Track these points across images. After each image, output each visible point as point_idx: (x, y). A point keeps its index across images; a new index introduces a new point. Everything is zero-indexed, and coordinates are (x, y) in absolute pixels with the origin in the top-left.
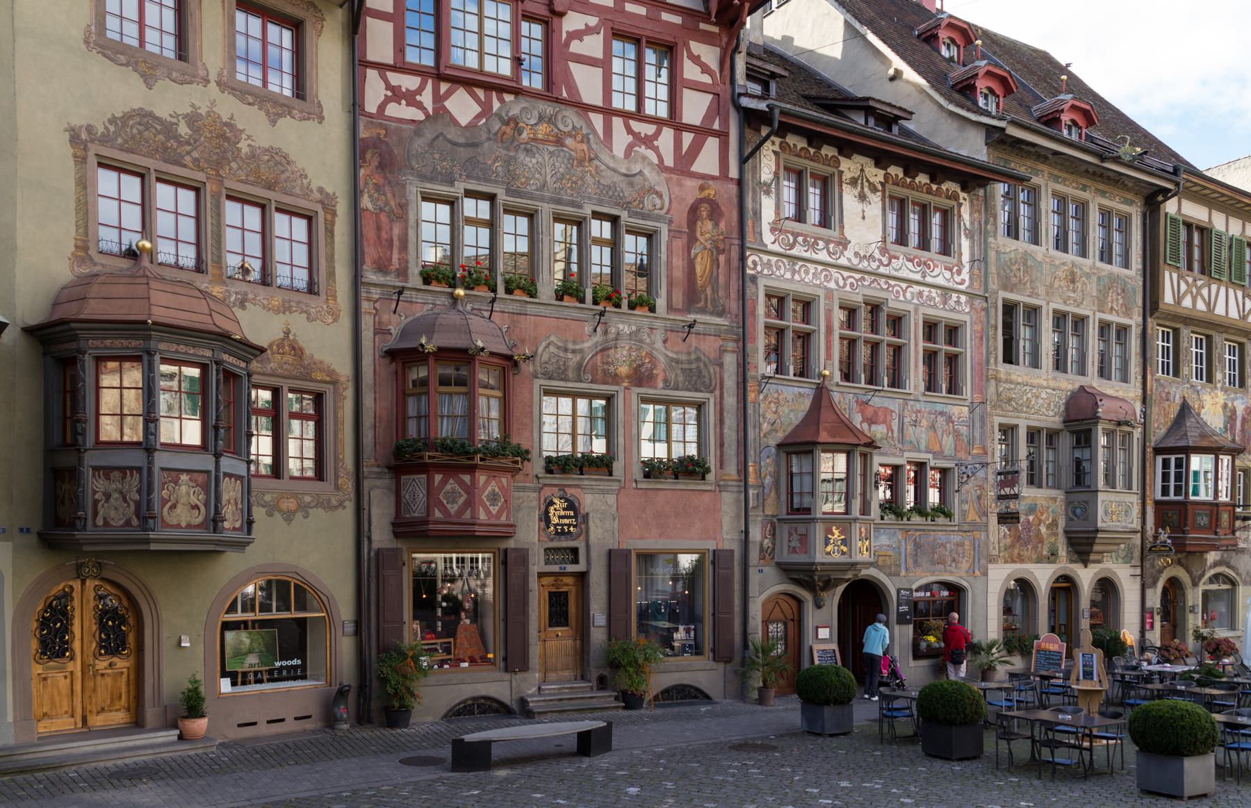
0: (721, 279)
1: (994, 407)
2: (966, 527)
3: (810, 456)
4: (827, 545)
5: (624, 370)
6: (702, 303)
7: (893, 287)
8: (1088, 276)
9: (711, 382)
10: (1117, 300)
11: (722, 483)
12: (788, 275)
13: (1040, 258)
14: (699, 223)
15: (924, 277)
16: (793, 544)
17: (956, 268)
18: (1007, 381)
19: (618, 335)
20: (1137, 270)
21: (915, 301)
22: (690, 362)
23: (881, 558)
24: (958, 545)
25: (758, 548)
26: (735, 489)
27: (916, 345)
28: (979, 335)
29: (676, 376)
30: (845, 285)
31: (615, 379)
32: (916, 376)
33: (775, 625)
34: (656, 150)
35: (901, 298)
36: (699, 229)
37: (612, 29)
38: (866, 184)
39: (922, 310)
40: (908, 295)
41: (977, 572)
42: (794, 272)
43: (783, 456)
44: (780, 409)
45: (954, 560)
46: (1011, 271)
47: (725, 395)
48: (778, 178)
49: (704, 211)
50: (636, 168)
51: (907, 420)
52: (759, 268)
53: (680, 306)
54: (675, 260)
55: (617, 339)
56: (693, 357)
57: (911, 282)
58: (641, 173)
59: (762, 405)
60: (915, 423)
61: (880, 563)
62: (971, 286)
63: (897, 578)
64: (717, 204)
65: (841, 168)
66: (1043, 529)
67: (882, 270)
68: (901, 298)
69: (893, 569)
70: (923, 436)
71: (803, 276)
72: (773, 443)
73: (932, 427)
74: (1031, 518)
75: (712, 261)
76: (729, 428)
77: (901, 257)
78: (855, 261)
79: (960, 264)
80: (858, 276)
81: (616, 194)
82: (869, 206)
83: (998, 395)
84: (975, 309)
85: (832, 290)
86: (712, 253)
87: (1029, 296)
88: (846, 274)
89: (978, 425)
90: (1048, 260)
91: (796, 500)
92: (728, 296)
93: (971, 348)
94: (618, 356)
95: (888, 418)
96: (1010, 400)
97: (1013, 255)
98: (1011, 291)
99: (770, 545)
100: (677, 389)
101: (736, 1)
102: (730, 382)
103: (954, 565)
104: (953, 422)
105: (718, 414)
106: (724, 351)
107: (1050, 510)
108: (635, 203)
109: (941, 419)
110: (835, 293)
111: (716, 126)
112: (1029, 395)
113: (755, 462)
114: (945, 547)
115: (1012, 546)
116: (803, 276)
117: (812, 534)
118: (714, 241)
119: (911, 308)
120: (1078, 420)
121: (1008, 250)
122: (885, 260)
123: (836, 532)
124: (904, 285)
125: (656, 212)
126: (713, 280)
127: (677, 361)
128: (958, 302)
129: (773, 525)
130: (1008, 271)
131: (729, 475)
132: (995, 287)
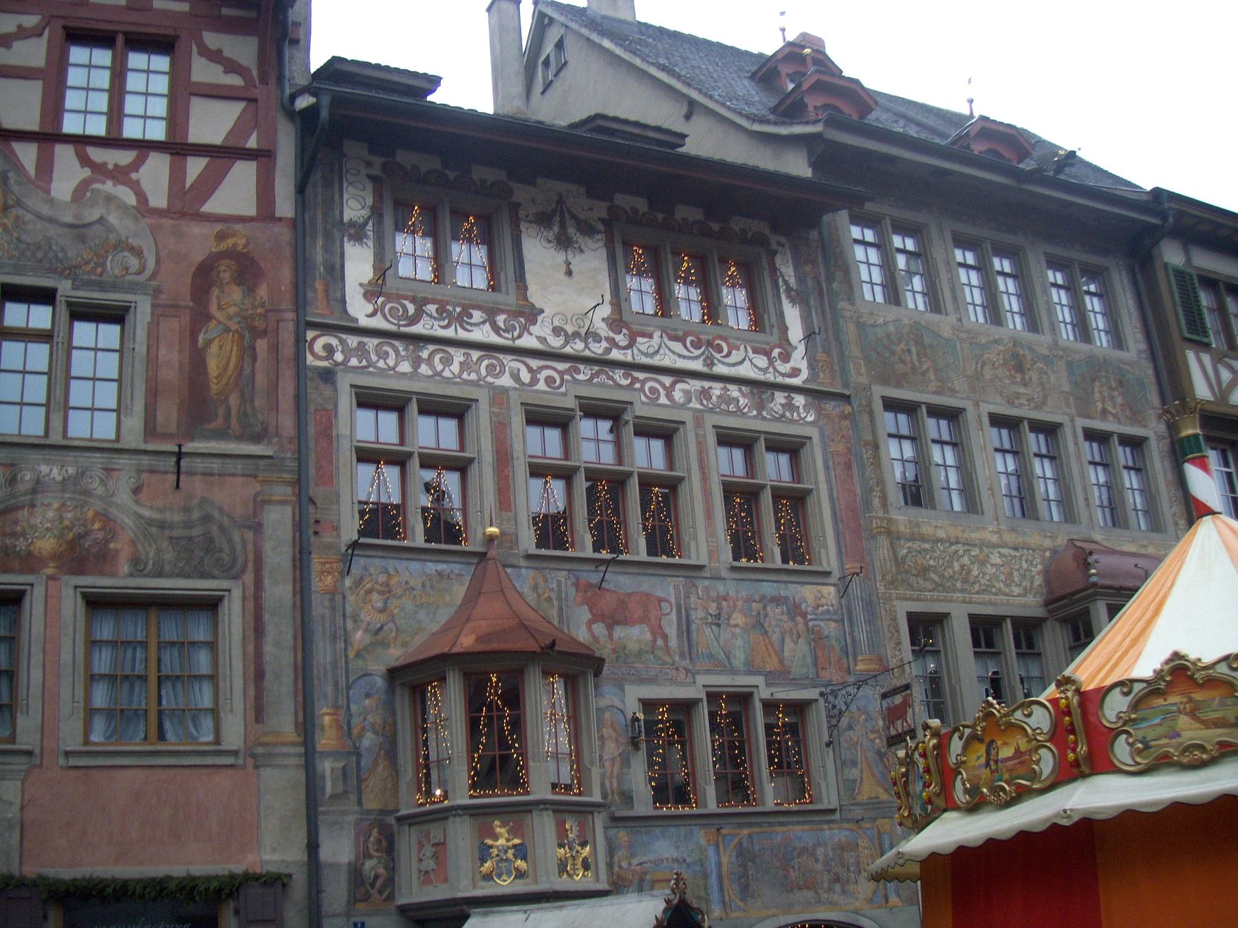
0: (261, 380)
1: (892, 583)
2: (858, 812)
4: (483, 860)
5: (46, 545)
6: (220, 421)
7: (643, 382)
8: (1047, 360)
9: (234, 560)
10: (1112, 398)
11: (260, 750)
12: (405, 367)
13: (947, 332)
14: (215, 292)
15: (710, 362)
17: (776, 352)
18: (913, 538)
19: (38, 486)
20: (1140, 352)
21: (695, 404)
22: (188, 525)
24: (842, 848)
25: (344, 877)
28: (841, 460)
29: (159, 551)
30: (534, 381)
31: (30, 562)
32: (711, 533)
34: (136, 188)
35: (663, 400)
36: (214, 301)
37: (65, 28)
38: (567, 216)
39: (711, 420)
40: (678, 395)
42: (417, 363)
43: (403, 703)
44: (393, 603)
45: (837, 879)
46: (893, 353)
47: (266, 581)
48: (381, 216)
49: (225, 272)
50: (93, 214)
51: (697, 615)
52: (339, 357)
53: (173, 429)
54: (163, 352)
55: (34, 491)
56: (196, 515)
57: (681, 374)
58: (101, 220)
59: (351, 598)
60: (717, 621)
64: (252, 259)
67: (616, 355)
68: (663, 400)
70: (739, 642)
71: (439, 367)
72: (378, 667)
73: (759, 625)
77: (657, 334)
78: (556, 342)
79: (785, 343)
80: (562, 366)
81: (51, 254)
83: (899, 562)
84: (828, 416)
85: (505, 390)
87: (934, 393)
88: (535, 363)
89: (861, 617)
90: (963, 336)
92: (274, 407)
93: (829, 482)
94: (37, 521)
96: (924, 571)
97: (891, 328)
98: (898, 385)
99: (381, 871)
100: (160, 575)
102: (278, 555)
103: (838, 887)
104: (804, 615)
105: (250, 619)
106: (264, 502)
108: (88, 267)
109: (775, 612)
110: (515, 398)
111: (252, 143)
112: (966, 560)
113: (336, 707)
114: (813, 854)
116: (439, 367)
118: (245, 318)
119: (686, 416)
120: (1063, 597)
121: (881, 321)
122: (621, 339)
124: (667, 380)
125: (128, 278)
126: (243, 382)
127: (162, 525)
128: (789, 406)
132: (864, 380)
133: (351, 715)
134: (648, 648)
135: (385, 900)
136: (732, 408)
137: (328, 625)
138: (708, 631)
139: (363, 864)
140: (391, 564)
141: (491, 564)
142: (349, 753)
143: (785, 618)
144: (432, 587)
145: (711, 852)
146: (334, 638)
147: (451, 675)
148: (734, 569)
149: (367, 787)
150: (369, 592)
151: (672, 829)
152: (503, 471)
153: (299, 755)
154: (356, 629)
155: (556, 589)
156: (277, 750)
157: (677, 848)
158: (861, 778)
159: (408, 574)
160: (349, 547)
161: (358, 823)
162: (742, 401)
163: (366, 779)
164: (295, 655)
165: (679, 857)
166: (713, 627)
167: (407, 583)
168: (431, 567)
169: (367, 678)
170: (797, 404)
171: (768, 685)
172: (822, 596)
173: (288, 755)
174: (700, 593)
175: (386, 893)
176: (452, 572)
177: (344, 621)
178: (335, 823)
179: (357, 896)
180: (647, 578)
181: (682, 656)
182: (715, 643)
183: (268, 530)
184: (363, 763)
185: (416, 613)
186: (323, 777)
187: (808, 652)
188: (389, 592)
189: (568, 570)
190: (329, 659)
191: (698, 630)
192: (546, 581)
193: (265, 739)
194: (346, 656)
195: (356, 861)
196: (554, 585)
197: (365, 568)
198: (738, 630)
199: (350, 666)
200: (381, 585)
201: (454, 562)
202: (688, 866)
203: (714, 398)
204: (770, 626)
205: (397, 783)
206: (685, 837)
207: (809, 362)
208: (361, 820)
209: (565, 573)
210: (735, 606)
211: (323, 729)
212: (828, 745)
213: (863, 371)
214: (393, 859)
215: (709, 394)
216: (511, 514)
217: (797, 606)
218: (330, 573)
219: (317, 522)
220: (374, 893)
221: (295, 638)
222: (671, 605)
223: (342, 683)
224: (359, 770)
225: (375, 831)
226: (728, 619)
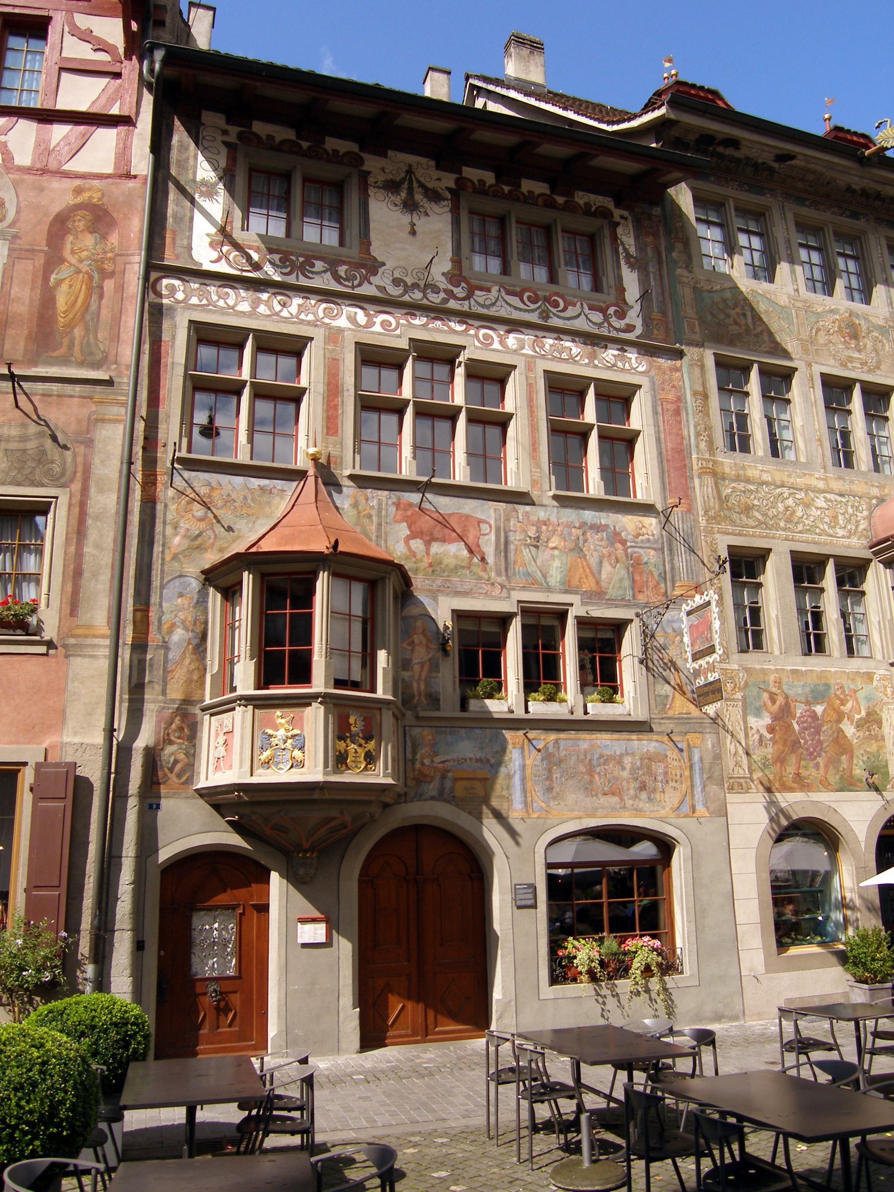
13: (783, 300)
18: (738, 479)
23: (460, 785)
28: (671, 407)
41: (700, 809)
45: (643, 787)
46: (728, 316)
59: (172, 507)
62: (646, 334)
65: (365, 168)
66: (849, 730)
74: (819, 709)
75: (90, 290)
78: (395, 291)
82: (424, 219)
85: (340, 330)
86: (91, 278)
99: (182, 756)
101: (892, 1096)
103: (644, 795)
104: (623, 542)
107: (860, 695)
109: (593, 538)
112: (790, 502)
114: (620, 762)
115: (781, 760)
130: (721, 316)
131: (90, 627)
133: (163, 612)
135: (183, 783)
139: (162, 749)
149: (172, 678)
151: (478, 731)
157: (482, 749)
162: (575, 351)
163: (173, 671)
169: (182, 580)
172: (643, 526)
183: (98, 445)
184: (170, 656)
191: (516, 550)
193: (79, 631)
194: (163, 559)
199: (166, 568)
208: (164, 708)
214: (194, 746)
224: (166, 661)
225: (178, 718)
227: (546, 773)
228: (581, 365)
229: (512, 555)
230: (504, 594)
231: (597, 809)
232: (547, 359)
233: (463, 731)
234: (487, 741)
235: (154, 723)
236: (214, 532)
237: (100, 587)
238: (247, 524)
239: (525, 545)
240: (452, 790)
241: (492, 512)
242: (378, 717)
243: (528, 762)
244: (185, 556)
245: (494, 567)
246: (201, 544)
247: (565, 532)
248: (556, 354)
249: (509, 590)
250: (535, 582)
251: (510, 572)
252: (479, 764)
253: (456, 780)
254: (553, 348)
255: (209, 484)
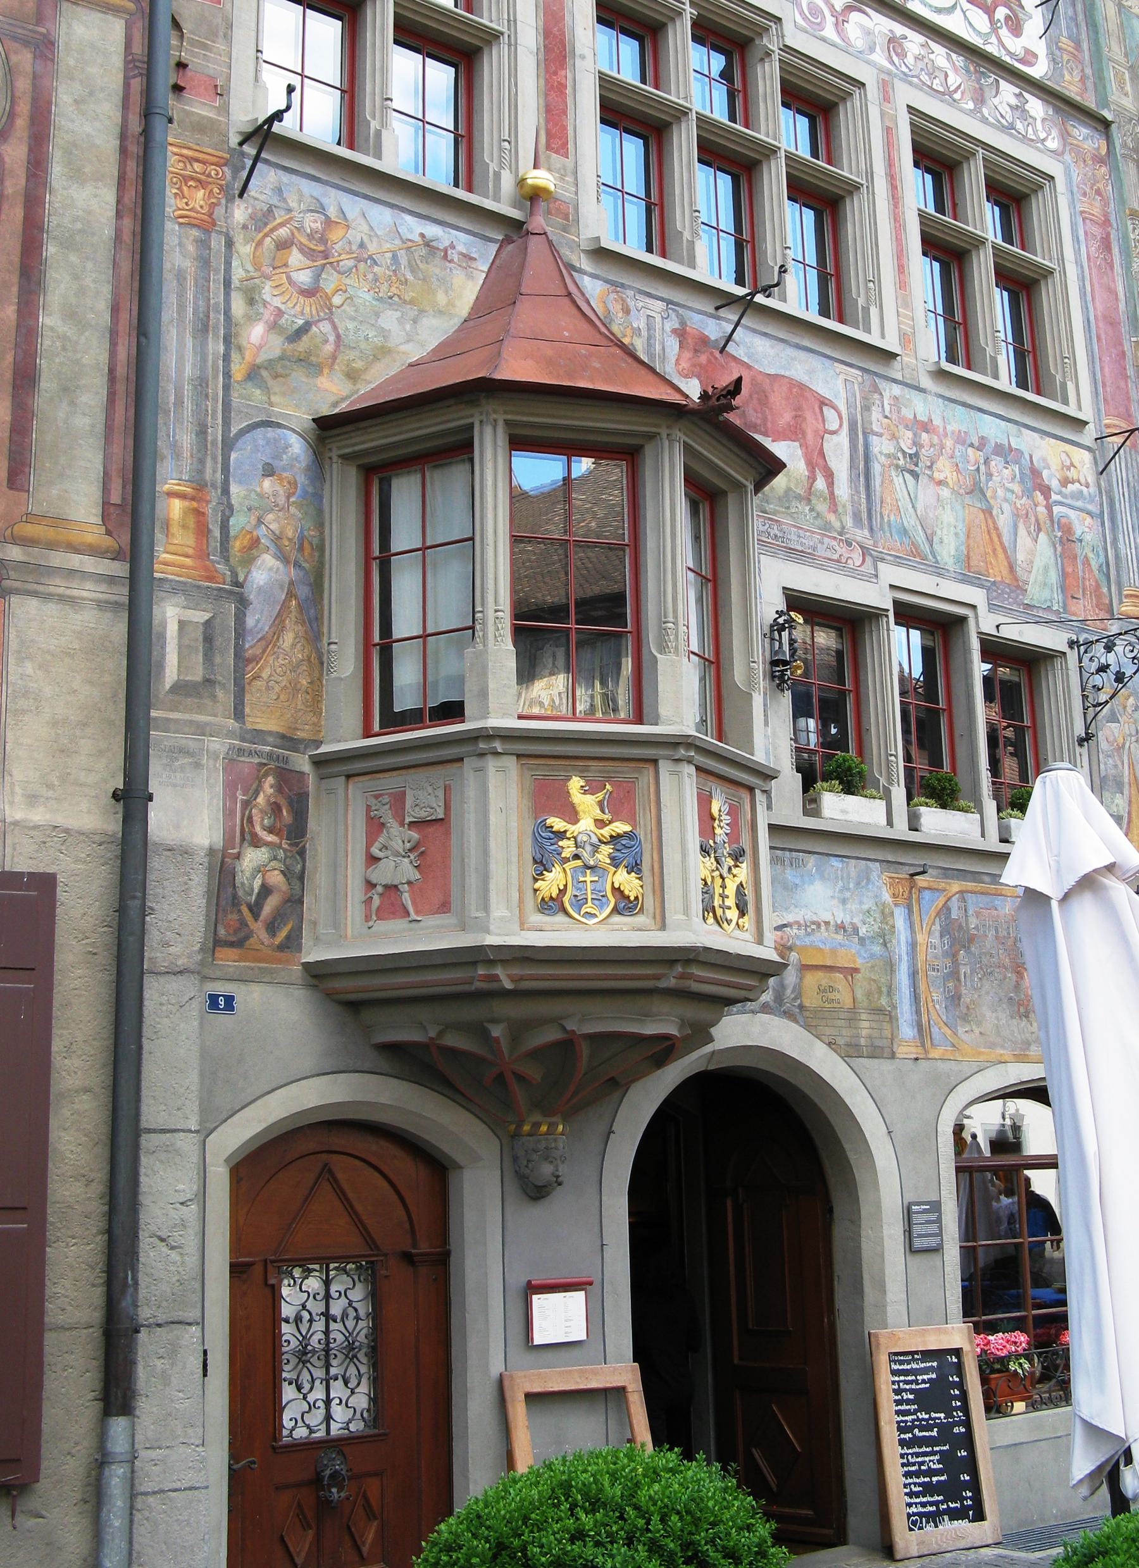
3: (457, 474)
4: (542, 865)
16: (384, 874)
21: (879, 57)
23: (811, 980)
25: (198, 882)
26: (88, 591)
27: (895, 199)
33: (313, 1284)
39: (905, 95)
51: (881, 446)
59: (244, 249)
61: (811, 1000)
63: (886, 1066)
69: (865, 1026)
76: (71, 315)
91: (406, 674)
95: (811, 424)
99: (276, 878)
104: (1046, 491)
117: (471, 818)
123: (587, 804)
129: (287, 778)
131: (59, 521)
133: (230, 507)
134: (800, 491)
135: (281, 948)
136: (937, 84)
137: (190, 295)
138: (898, 481)
139: (238, 856)
140: (336, 200)
141: (534, 243)
142: (221, 595)
143: (1016, 487)
144: (413, 268)
145: (900, 919)
146: (203, 328)
147: (488, 430)
148: (941, 375)
149: (257, 677)
150: (283, 245)
151: (836, 863)
152: (555, 73)
153: (111, 580)
154: (251, 319)
155: (644, 333)
156: (58, 559)
157: (844, 901)
158: (1129, 813)
159: (365, 228)
160: (246, 138)
161: (230, 763)
162: (954, 80)
163: (255, 659)
164: (113, 344)
165: (847, 921)
166: (907, 476)
167: (362, 245)
168: (414, 227)
169: (270, 432)
170: (1033, 113)
171: (992, 608)
172: (1072, 465)
173: (84, 575)
174: (887, 408)
175: (283, 934)
176: (453, 247)
177: (227, 295)
178: (184, 751)
179: (222, 932)
180: (802, 355)
181: (857, 517)
182: (911, 510)
183: (67, 59)
184: (250, 622)
185: (377, 315)
186: (162, 636)
187: (1053, 560)
188: (326, 255)
189: (669, 302)
190: (188, 371)
191: (883, 475)
192: (627, 311)
193: (30, 530)
194: (227, 375)
195: (225, 849)
196: (642, 324)
197: (279, 191)
198: (945, 493)
199: (235, 400)
200: (310, 237)
201: (457, 228)
202: (862, 941)
203: (910, 60)
204: (994, 497)
205: (320, 680)
206: (858, 884)
207: (1048, 47)
208: (241, 751)
209: (659, 305)
210: (942, 447)
211: (167, 524)
212: (1081, 741)
213: (1128, 88)
214: (302, 853)
215: (901, 45)
216: (569, 162)
217: (1035, 473)
218: (202, 184)
219: (181, 66)
220: (258, 928)
221: (115, 309)
222: (840, 418)
223: (216, 433)
224: (241, 631)
225: (270, 780)
226: (930, 467)
227: (948, 962)
228: (962, 110)
229: (877, 482)
230: (868, 568)
231: (1029, 1044)
232: (911, 84)
233: (812, 860)
234: (851, 886)
235: (219, 788)
236: (335, 327)
237: (82, 422)
238: (401, 321)
239: (897, 467)
240: (799, 992)
241: (840, 383)
242: (748, 807)
243: (921, 938)
244: (276, 376)
245: (849, 508)
246: (309, 353)
247: (957, 454)
248: (925, 77)
249: (877, 560)
250: (916, 551)
251: (876, 523)
252: (839, 937)
253: (805, 968)
254: (920, 65)
255: (320, 209)
